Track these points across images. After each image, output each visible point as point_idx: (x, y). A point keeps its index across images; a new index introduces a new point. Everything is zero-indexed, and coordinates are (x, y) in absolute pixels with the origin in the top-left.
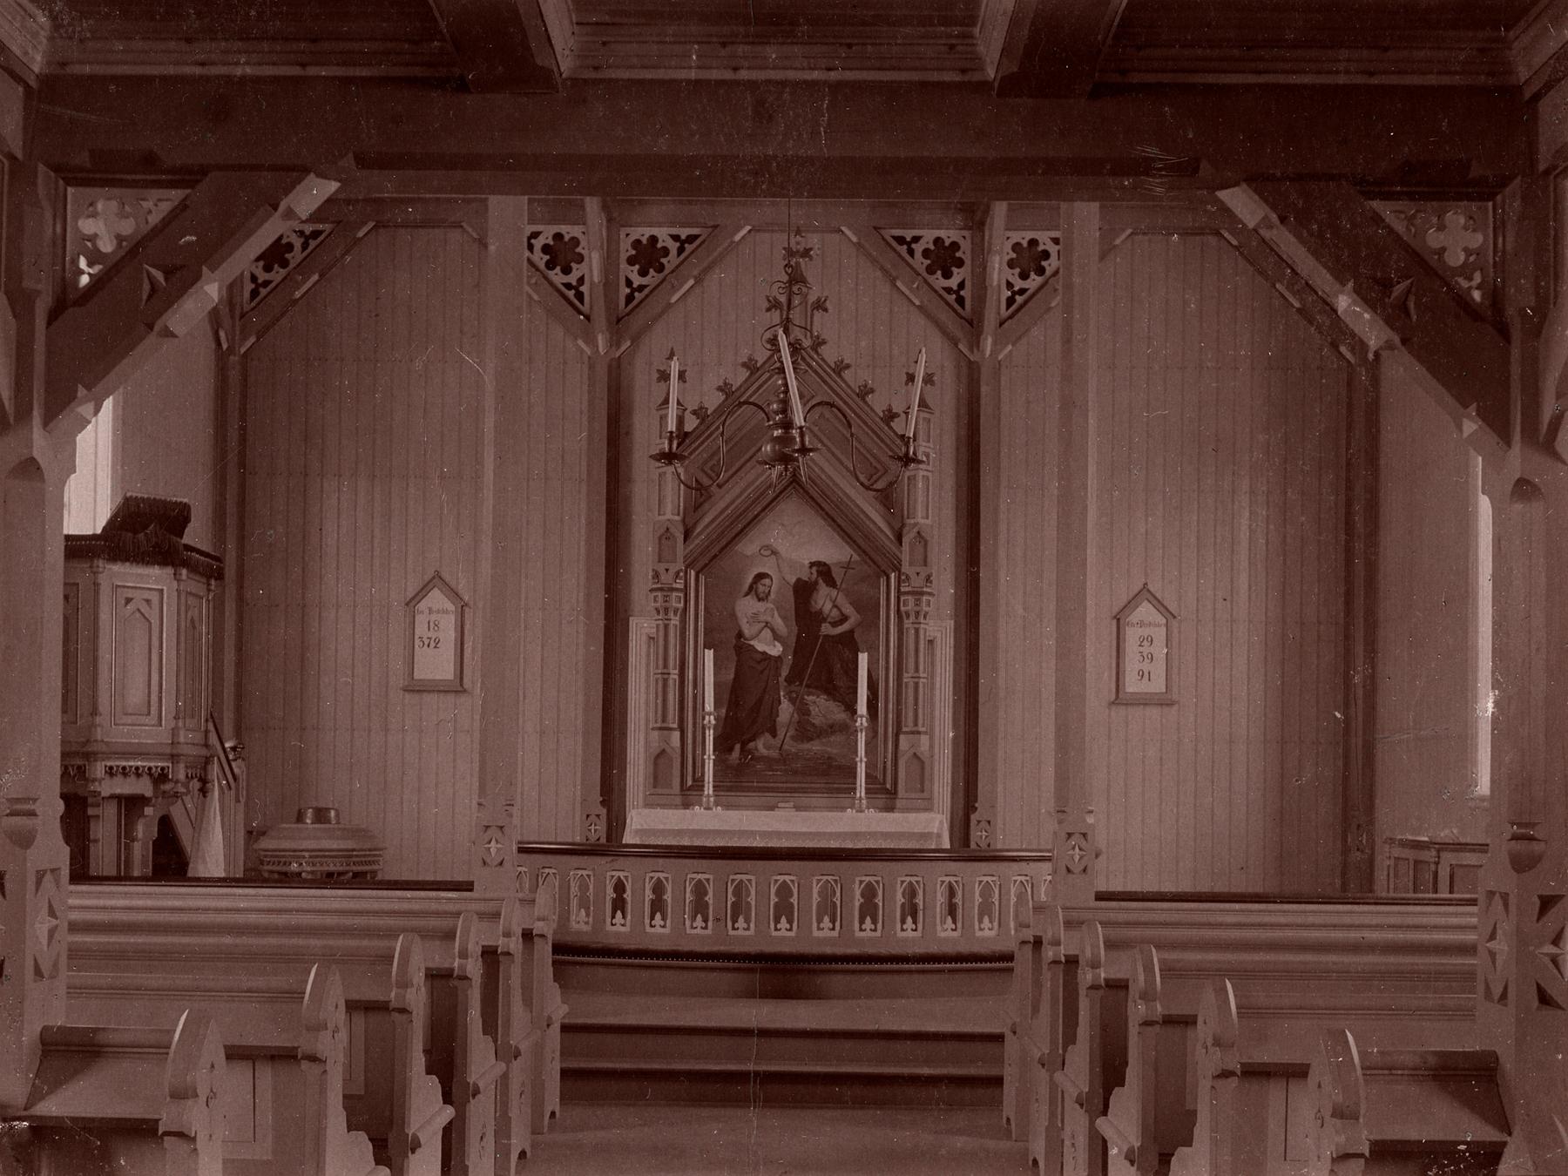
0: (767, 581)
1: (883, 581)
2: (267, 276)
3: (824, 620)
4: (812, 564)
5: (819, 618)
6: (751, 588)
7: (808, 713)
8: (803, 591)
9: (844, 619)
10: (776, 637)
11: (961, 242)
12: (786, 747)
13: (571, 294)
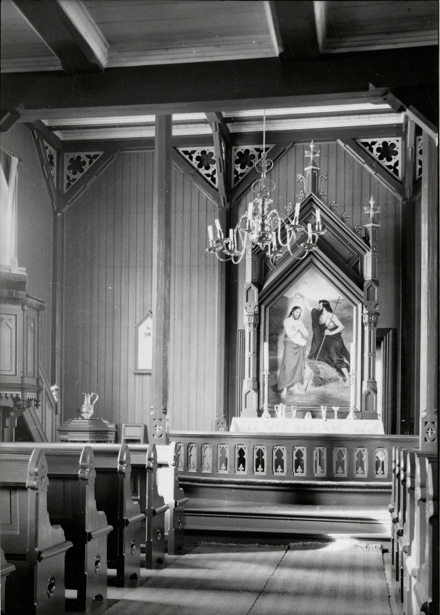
0: (298, 310)
1: (355, 308)
2: (74, 177)
3: (326, 328)
4: (320, 302)
5: (323, 327)
6: (291, 314)
7: (319, 373)
8: (316, 314)
9: (336, 327)
10: (303, 337)
11: (69, 158)
12: (308, 389)
13: (209, 179)
